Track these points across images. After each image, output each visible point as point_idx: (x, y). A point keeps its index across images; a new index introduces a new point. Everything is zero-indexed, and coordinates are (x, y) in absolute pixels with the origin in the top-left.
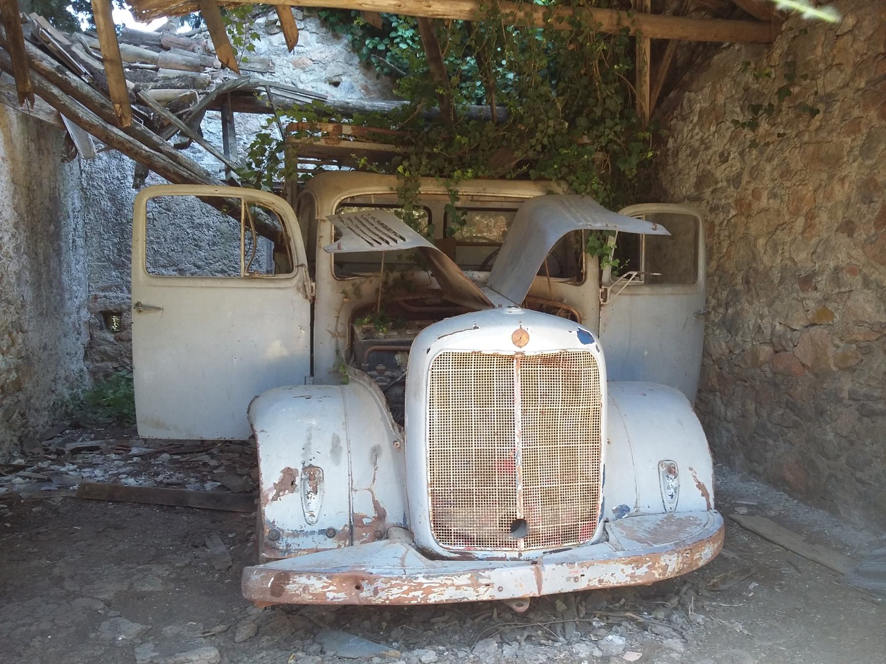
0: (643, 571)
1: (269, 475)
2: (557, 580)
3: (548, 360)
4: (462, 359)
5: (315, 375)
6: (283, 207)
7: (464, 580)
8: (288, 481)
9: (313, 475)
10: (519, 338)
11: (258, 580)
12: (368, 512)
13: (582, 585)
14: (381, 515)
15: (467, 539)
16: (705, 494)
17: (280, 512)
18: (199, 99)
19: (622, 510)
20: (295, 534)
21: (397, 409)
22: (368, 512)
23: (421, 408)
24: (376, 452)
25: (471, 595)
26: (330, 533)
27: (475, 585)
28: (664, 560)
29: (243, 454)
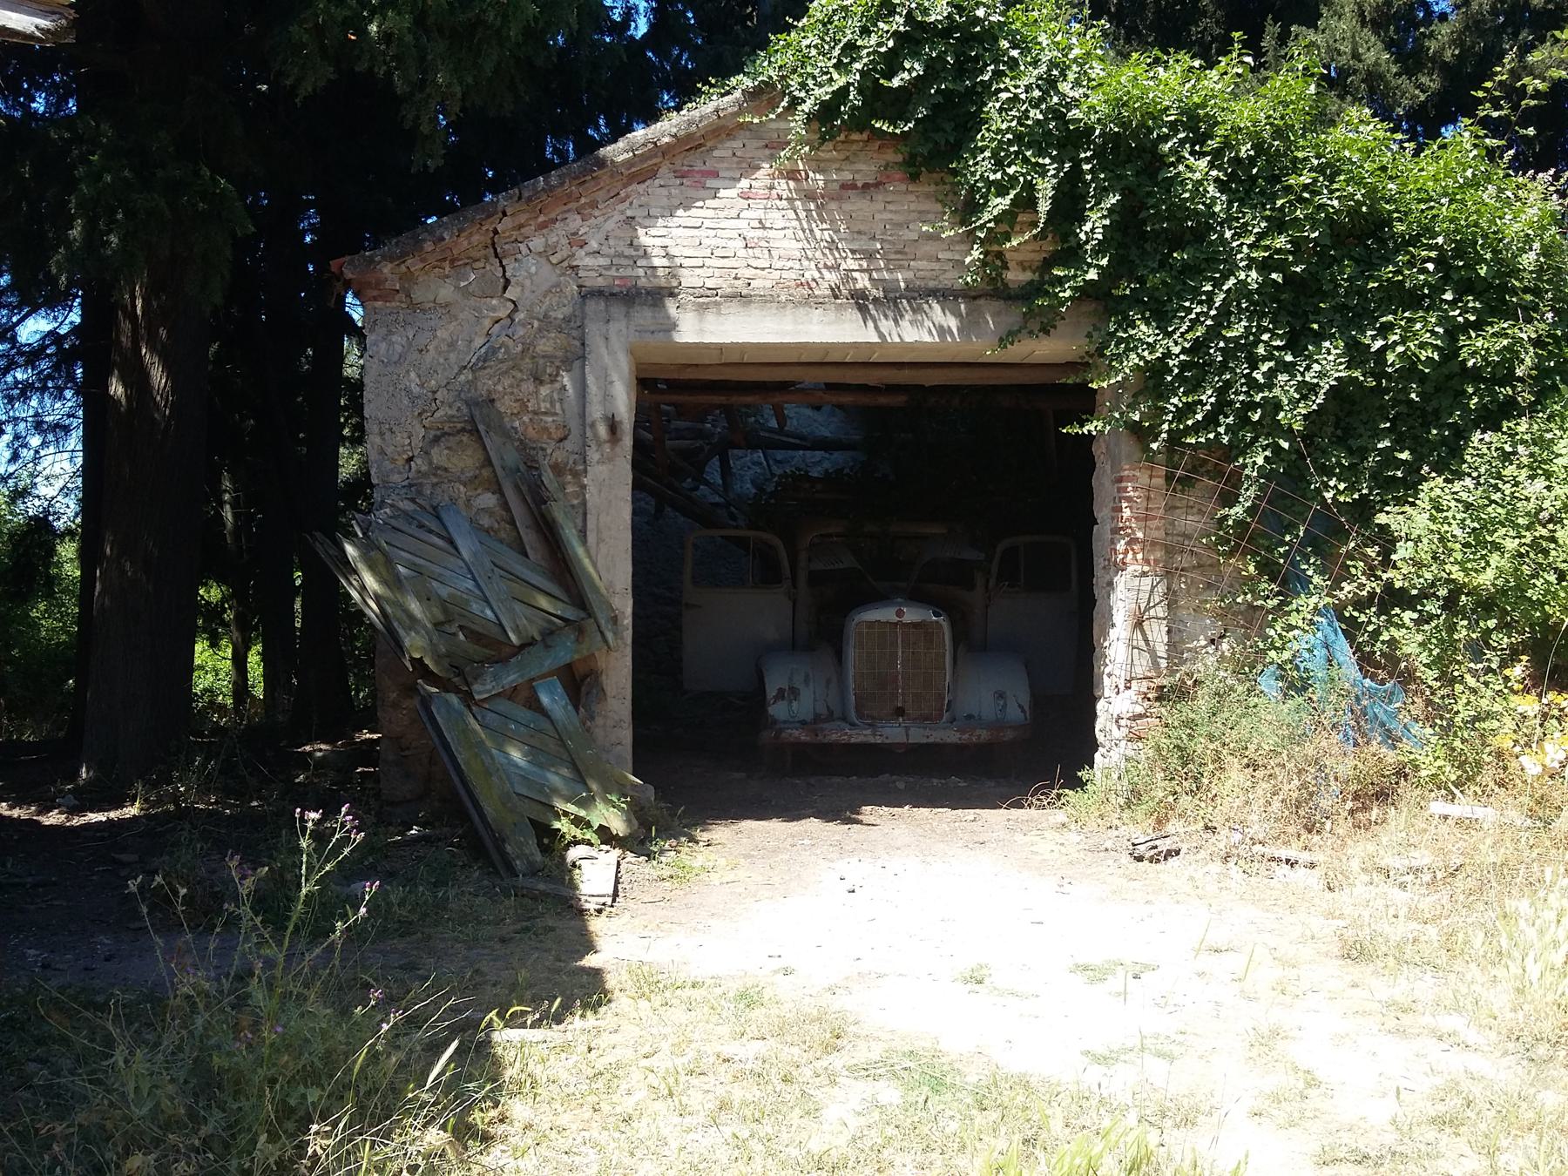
0: (966, 736)
1: (771, 692)
2: (918, 735)
3: (915, 625)
4: (871, 624)
5: (795, 645)
6: (777, 542)
7: (868, 732)
8: (781, 695)
9: (794, 692)
10: (900, 614)
11: (767, 736)
12: (823, 711)
13: (931, 740)
14: (831, 713)
15: (873, 718)
16: (1023, 711)
17: (778, 710)
18: (707, 448)
19: (970, 717)
20: (709, 300)
21: (839, 655)
22: (823, 711)
23: (851, 654)
24: (828, 682)
25: (872, 740)
26: (803, 723)
27: (874, 735)
28: (978, 732)
29: (756, 698)
